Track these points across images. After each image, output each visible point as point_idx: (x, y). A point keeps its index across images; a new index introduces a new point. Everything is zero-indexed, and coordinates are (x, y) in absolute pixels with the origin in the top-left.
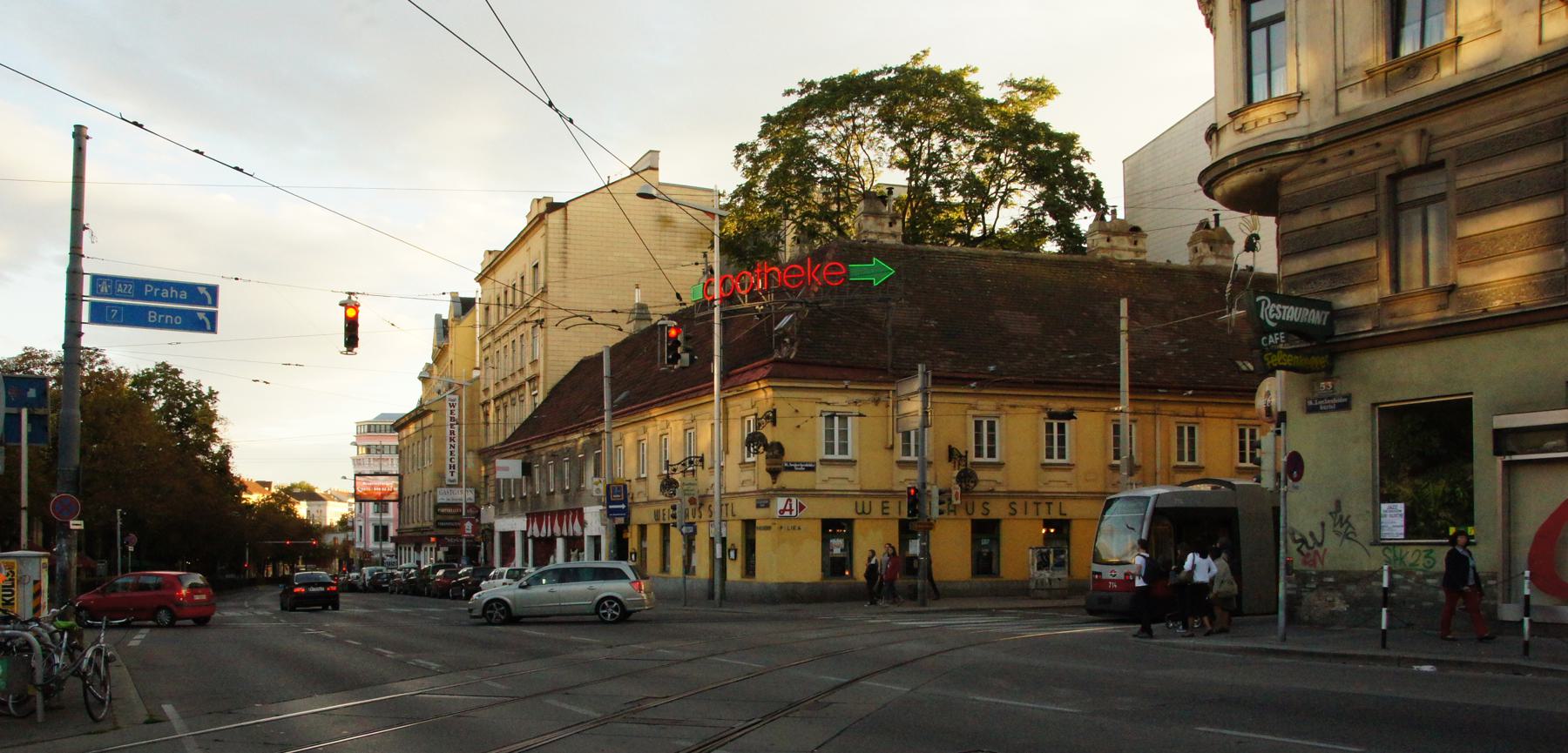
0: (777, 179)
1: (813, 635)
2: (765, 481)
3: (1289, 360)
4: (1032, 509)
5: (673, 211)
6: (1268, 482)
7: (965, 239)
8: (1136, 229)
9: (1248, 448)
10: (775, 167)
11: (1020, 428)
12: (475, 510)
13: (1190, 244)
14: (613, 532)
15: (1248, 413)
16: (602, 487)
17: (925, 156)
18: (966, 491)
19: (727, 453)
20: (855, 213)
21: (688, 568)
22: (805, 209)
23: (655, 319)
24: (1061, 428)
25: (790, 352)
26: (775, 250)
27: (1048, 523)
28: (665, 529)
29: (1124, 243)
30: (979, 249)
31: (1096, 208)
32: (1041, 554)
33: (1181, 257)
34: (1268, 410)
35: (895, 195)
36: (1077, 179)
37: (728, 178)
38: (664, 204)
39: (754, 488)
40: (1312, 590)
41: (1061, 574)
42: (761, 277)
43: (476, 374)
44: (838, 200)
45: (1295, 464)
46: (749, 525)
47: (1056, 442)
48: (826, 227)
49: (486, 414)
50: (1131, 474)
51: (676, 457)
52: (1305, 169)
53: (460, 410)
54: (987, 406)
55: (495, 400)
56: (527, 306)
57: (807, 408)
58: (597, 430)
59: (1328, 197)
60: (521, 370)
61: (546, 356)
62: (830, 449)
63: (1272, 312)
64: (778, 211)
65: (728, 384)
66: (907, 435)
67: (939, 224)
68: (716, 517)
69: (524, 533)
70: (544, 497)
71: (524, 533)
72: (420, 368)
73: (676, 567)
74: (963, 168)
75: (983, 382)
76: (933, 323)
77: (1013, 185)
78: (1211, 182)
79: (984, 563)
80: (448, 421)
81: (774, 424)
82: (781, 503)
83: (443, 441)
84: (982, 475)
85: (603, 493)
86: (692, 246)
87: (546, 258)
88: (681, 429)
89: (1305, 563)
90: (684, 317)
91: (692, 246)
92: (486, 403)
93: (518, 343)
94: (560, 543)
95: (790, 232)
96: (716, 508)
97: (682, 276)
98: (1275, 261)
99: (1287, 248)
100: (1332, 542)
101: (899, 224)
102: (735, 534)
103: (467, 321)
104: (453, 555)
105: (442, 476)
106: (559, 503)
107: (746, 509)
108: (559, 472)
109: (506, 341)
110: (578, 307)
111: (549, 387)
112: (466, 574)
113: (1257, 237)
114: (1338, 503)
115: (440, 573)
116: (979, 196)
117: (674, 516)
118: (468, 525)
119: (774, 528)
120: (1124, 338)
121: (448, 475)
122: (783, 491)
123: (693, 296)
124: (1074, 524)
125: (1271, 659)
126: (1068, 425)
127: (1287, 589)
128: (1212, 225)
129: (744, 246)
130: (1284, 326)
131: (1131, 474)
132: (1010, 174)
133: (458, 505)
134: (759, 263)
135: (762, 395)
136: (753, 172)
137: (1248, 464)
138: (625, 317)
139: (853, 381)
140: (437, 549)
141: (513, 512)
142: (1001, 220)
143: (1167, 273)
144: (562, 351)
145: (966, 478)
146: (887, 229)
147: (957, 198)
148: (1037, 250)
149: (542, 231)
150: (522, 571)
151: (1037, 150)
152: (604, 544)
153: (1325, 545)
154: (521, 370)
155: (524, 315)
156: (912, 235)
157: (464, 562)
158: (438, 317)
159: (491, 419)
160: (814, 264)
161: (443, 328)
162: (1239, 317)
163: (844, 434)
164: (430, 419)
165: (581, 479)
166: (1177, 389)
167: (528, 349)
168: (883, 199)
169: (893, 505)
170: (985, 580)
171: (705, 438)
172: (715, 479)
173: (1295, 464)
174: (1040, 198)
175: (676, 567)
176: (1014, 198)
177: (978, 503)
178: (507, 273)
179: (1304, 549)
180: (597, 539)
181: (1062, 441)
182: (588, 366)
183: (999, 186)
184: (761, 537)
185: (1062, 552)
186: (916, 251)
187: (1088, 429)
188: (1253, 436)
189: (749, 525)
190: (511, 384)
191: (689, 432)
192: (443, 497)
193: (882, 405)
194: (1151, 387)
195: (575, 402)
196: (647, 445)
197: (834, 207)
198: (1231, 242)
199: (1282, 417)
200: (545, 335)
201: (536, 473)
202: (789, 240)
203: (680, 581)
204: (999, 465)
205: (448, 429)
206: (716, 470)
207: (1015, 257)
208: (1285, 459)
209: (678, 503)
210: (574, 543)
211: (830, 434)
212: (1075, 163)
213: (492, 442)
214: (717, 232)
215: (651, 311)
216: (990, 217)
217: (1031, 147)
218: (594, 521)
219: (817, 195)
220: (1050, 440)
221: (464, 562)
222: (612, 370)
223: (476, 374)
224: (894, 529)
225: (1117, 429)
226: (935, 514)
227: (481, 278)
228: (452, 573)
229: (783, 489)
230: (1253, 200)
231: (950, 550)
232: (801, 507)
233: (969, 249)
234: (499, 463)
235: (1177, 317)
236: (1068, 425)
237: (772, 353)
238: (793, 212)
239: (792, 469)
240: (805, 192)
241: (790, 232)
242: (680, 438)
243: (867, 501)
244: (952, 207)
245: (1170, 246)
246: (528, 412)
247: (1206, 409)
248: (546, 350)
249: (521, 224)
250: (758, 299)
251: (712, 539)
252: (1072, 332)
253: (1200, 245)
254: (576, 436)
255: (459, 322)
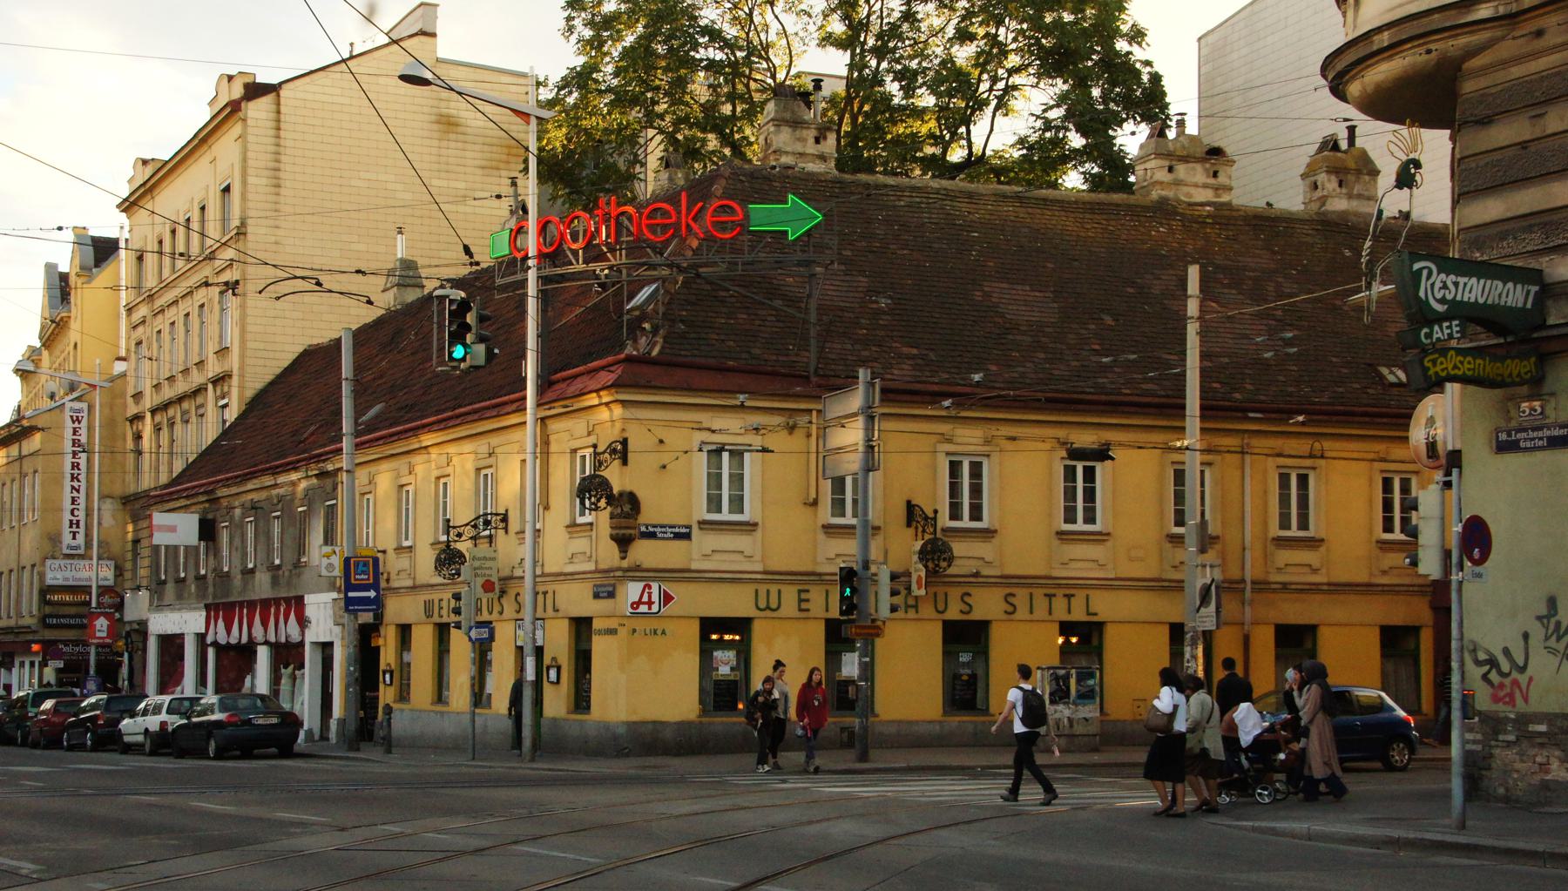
0: (638, 57)
1: (686, 807)
2: (609, 554)
3: (1467, 366)
4: (1041, 604)
5: (458, 108)
6: (1430, 566)
7: (938, 165)
8: (1216, 152)
9: (1397, 508)
10: (629, 39)
11: (1021, 474)
12: (114, 598)
13: (1304, 176)
14: (354, 638)
15: (1397, 452)
16: (337, 561)
17: (875, 29)
18: (933, 574)
19: (547, 508)
20: (761, 119)
21: (479, 697)
22: (682, 111)
23: (430, 285)
24: (1090, 474)
25: (652, 345)
26: (630, 177)
27: (1066, 628)
28: (442, 631)
29: (1194, 174)
30: (960, 183)
31: (1148, 118)
32: (1056, 678)
33: (1291, 199)
34: (1432, 447)
35: (826, 91)
36: (1120, 71)
37: (555, 56)
38: (446, 94)
39: (591, 566)
40: (1509, 744)
41: (1089, 711)
42: (606, 220)
43: (120, 367)
44: (732, 98)
45: (1476, 537)
46: (582, 627)
47: (1079, 495)
48: (713, 142)
49: (138, 437)
50: (1203, 550)
51: (462, 514)
52: (1506, 49)
53: (90, 428)
54: (969, 437)
55: (154, 412)
56: (211, 257)
57: (677, 438)
58: (330, 467)
59: (1537, 97)
60: (200, 364)
61: (243, 341)
62: (714, 503)
63: (1437, 287)
64: (636, 113)
65: (550, 395)
66: (839, 484)
67: (897, 141)
68: (527, 614)
69: (201, 638)
70: (237, 580)
71: (201, 638)
72: (16, 354)
73: (459, 695)
74: (939, 51)
75: (966, 398)
76: (883, 303)
77: (1016, 80)
78: (1341, 75)
79: (965, 693)
80: (68, 447)
81: (625, 462)
82: (633, 590)
83: (58, 482)
84: (959, 548)
85: (338, 571)
86: (490, 168)
87: (244, 174)
88: (470, 466)
89: (1496, 699)
90: (478, 283)
91: (490, 168)
92: (138, 418)
93: (194, 318)
94: (263, 654)
95: (655, 149)
96: (527, 598)
97: (474, 215)
98: (1448, 203)
99: (1470, 181)
100: (1542, 665)
101: (831, 139)
102: (558, 641)
103: (104, 276)
104: (73, 674)
105: (54, 539)
106: (262, 587)
107: (577, 600)
108: (263, 535)
109: (171, 314)
110: (299, 261)
111: (249, 394)
112: (93, 707)
113: (1417, 164)
114: (1552, 602)
115: (48, 704)
116: (962, 96)
117: (457, 611)
118: (102, 624)
119: (623, 632)
120: (1192, 329)
121: (67, 538)
122: (636, 572)
123: (491, 250)
124: (1110, 633)
125: (1443, 859)
126: (1100, 468)
127: (1464, 742)
128: (1344, 145)
129: (578, 172)
130: (1461, 312)
131: (1203, 550)
132: (1013, 60)
133: (86, 590)
134: (603, 198)
135: (604, 414)
136: (595, 44)
137: (1397, 535)
138: (381, 281)
139: (753, 393)
140: (43, 664)
141: (181, 601)
142: (1000, 134)
143: (1267, 224)
144: (268, 336)
145: (935, 553)
146: (811, 148)
147: (926, 100)
148: (1054, 185)
149: (237, 129)
150: (194, 701)
151: (1058, 23)
152: (339, 655)
153: (1529, 671)
154: (200, 364)
155: (206, 271)
156: (849, 160)
157: (91, 685)
158: (50, 268)
159: (147, 443)
160: (691, 202)
161: (61, 288)
162: (1383, 300)
163: (737, 480)
164: (36, 441)
165: (301, 548)
166: (1278, 412)
167: (212, 330)
168: (805, 97)
169: (816, 595)
170: (962, 721)
171: (511, 483)
172: (526, 551)
173: (1476, 537)
174: (1062, 99)
175: (459, 695)
176: (1017, 103)
177: (954, 593)
178: (175, 199)
179: (1494, 676)
180: (326, 647)
181: (1090, 495)
182: (318, 359)
183: (995, 80)
184: (600, 647)
185: (1092, 676)
186: (857, 184)
187: (1133, 476)
188: (1405, 489)
189: (582, 627)
190: (181, 387)
191: (484, 477)
192: (57, 574)
193: (800, 433)
194: (1236, 409)
195: (293, 420)
196: (411, 494)
197: (727, 109)
198: (1374, 173)
199: (1455, 460)
200: (243, 307)
201: (224, 537)
202: (653, 162)
203: (467, 719)
204: (988, 534)
205: (69, 459)
206: (528, 535)
207: (1018, 197)
208: (1458, 528)
209: (464, 590)
210: (287, 655)
211: (715, 480)
212: (1121, 45)
213: (147, 482)
214: (533, 147)
215: (423, 272)
216: (979, 131)
217: (1048, 18)
218: (323, 618)
219: (699, 87)
220: (1070, 494)
221: (91, 685)
222: (358, 368)
223: (120, 367)
224: (819, 631)
225: (1179, 477)
226: (884, 611)
227: (129, 205)
228: (68, 703)
229: (638, 568)
230: (1411, 103)
231: (906, 675)
232: (667, 598)
233: (945, 183)
234: (159, 518)
235: (1280, 297)
236: (1100, 468)
237: (622, 346)
238: (661, 117)
239: (652, 536)
240: (680, 84)
241: (655, 149)
242: (469, 484)
243: (774, 589)
244: (919, 113)
245: (1273, 180)
246: (211, 433)
247: (1327, 444)
248: (243, 331)
249: (203, 116)
250: (601, 257)
251: (520, 649)
252: (1109, 320)
253: (1322, 178)
254: (294, 476)
255: (90, 278)
